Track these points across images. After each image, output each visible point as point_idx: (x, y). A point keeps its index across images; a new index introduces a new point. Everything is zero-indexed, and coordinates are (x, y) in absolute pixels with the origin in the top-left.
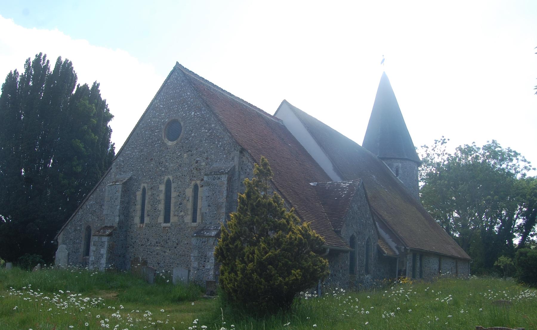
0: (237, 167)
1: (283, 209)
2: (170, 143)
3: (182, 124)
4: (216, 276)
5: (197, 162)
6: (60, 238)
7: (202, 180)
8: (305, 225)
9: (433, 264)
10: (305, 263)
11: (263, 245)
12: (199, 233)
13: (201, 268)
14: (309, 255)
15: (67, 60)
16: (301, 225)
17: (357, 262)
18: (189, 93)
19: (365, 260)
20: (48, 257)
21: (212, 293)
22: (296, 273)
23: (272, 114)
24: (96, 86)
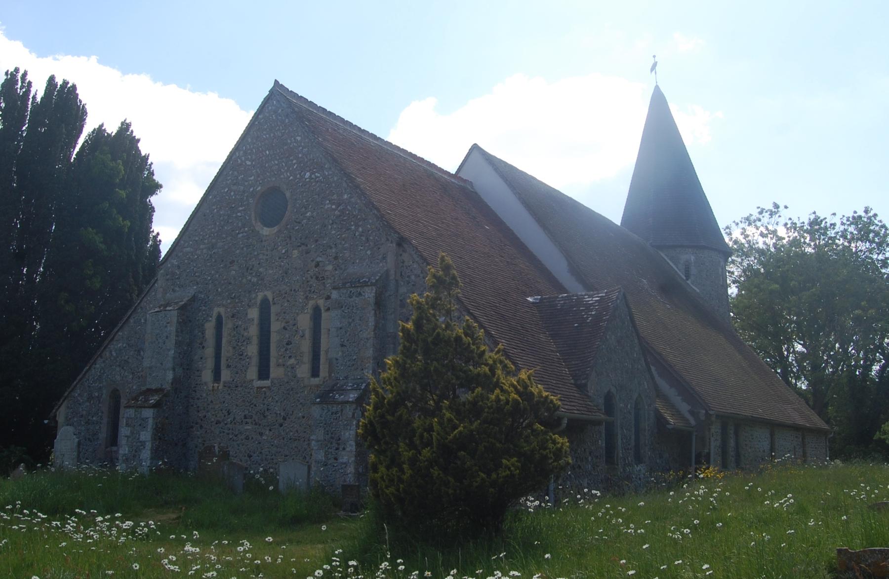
0: (392, 272)
1: (483, 348)
2: (266, 231)
3: (288, 194)
4: (358, 475)
5: (317, 265)
6: (62, 413)
7: (328, 298)
8: (523, 375)
9: (760, 440)
10: (525, 445)
11: (448, 415)
12: (325, 397)
13: (330, 462)
14: (533, 431)
15: (65, 83)
16: (514, 375)
17: (620, 440)
18: (299, 138)
19: (633, 437)
20: (38, 450)
21: (355, 508)
22: (511, 463)
23: (453, 170)
24: (125, 127)
